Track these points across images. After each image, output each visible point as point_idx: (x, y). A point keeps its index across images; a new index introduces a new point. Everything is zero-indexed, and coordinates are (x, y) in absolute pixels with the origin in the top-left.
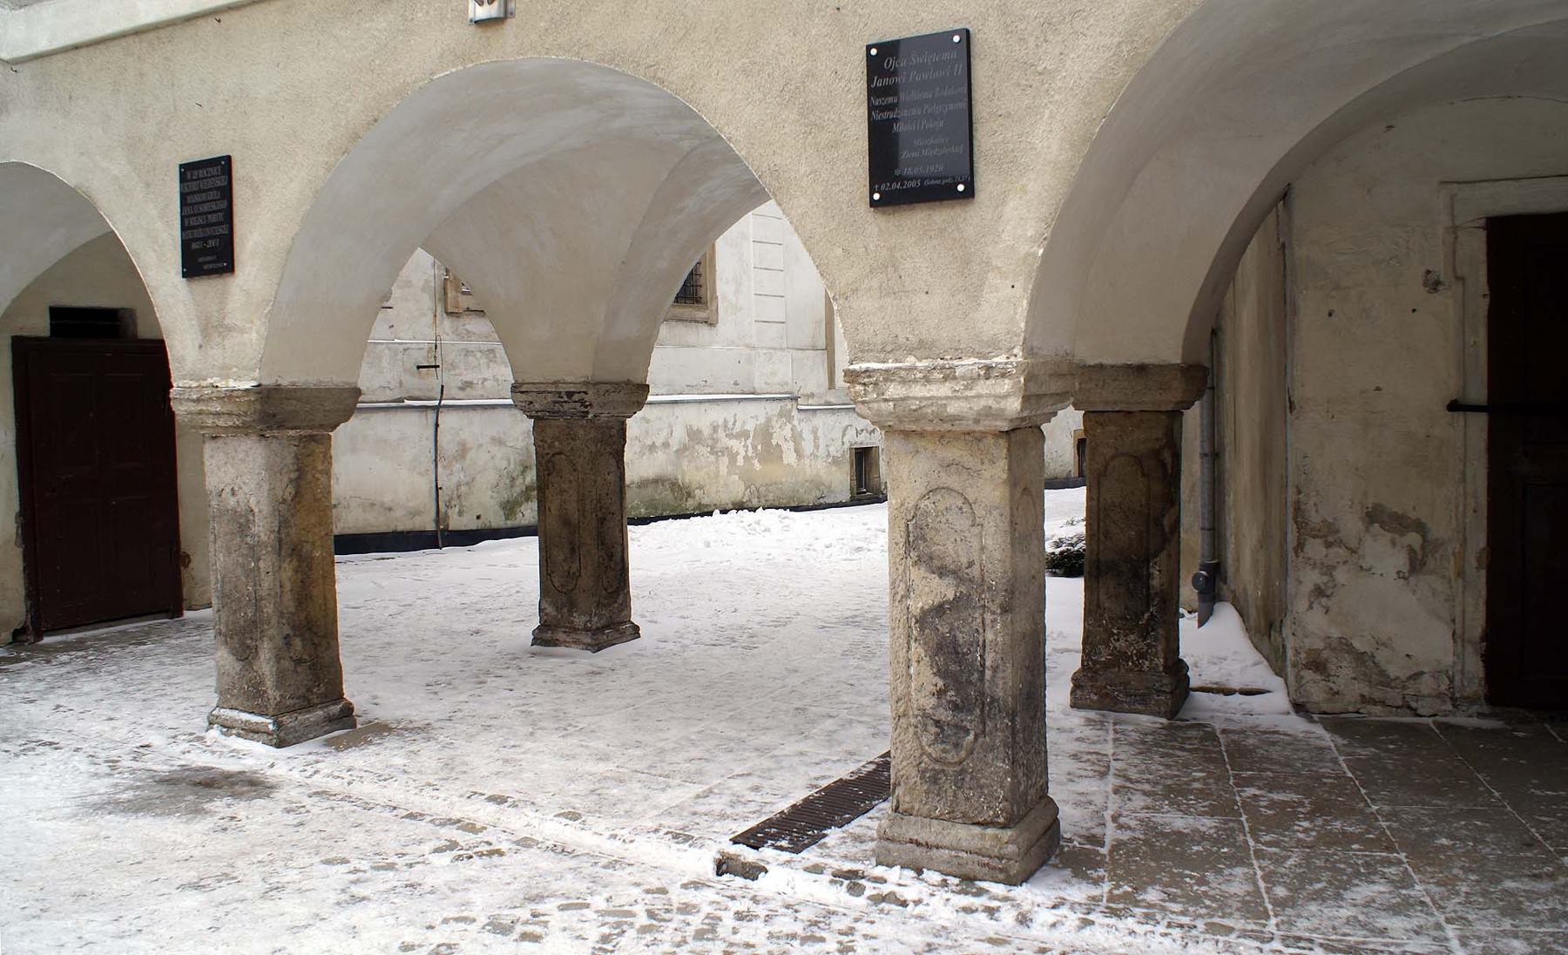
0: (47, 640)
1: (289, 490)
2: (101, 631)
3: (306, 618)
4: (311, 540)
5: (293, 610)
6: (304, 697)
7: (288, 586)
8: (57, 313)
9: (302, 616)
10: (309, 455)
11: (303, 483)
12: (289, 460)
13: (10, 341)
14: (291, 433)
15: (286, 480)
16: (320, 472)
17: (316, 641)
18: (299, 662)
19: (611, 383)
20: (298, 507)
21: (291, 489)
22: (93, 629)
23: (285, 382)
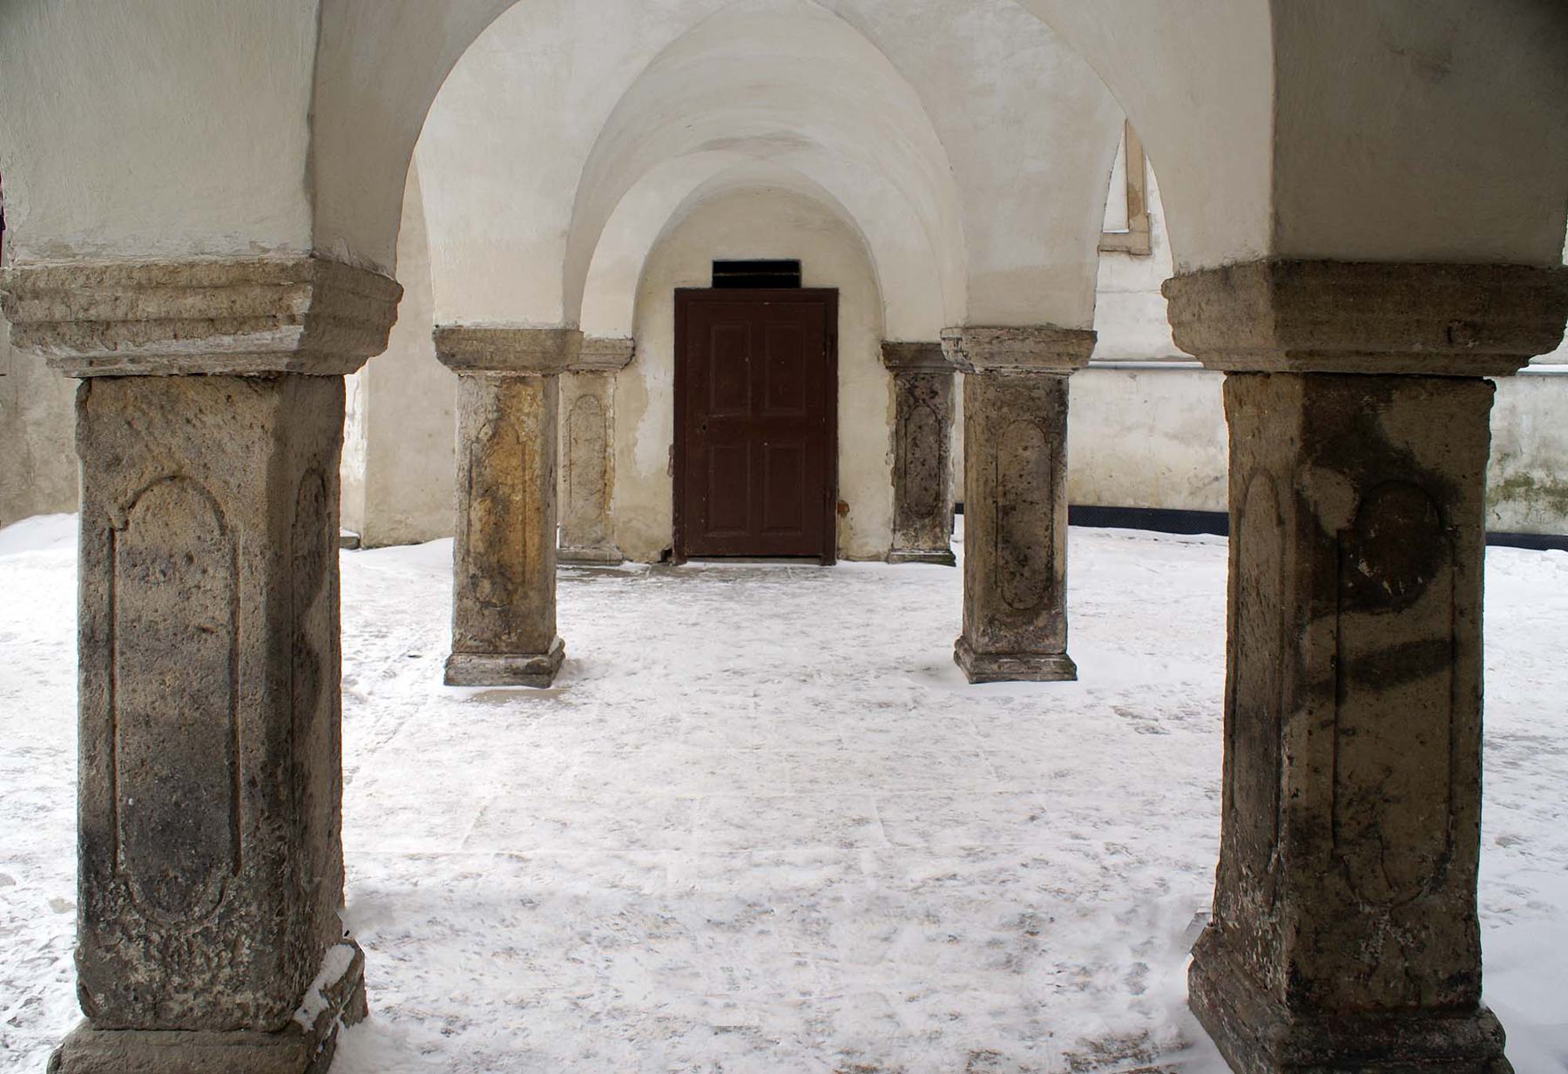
0: (690, 564)
1: (484, 430)
2: (728, 565)
3: (498, 561)
4: (510, 482)
5: (483, 551)
6: (490, 642)
7: (477, 526)
8: (719, 266)
9: (494, 559)
10: (514, 397)
11: (503, 424)
12: (489, 400)
13: (673, 293)
14: (490, 373)
15: (482, 419)
16: (528, 415)
17: (510, 587)
18: (486, 604)
19: (1002, 328)
20: (495, 448)
21: (488, 430)
22: (739, 562)
23: (467, 322)
